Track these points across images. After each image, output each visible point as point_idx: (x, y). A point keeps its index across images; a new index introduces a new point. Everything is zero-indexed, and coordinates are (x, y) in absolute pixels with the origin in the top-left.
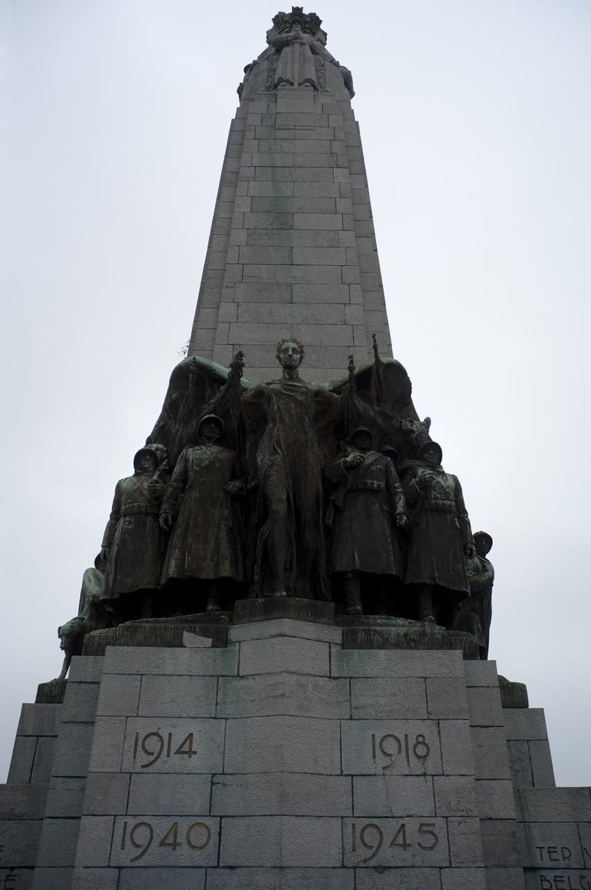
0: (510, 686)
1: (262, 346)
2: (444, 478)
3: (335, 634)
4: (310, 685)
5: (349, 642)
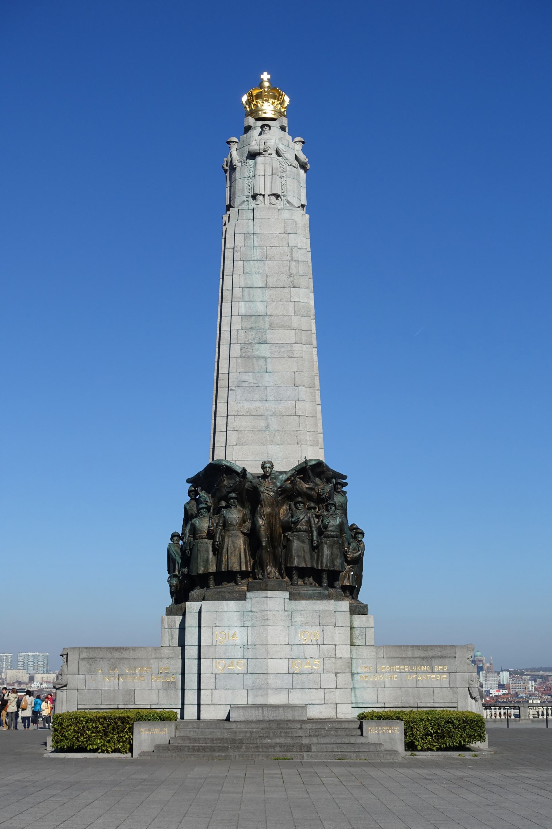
3: (287, 594)
5: (293, 597)
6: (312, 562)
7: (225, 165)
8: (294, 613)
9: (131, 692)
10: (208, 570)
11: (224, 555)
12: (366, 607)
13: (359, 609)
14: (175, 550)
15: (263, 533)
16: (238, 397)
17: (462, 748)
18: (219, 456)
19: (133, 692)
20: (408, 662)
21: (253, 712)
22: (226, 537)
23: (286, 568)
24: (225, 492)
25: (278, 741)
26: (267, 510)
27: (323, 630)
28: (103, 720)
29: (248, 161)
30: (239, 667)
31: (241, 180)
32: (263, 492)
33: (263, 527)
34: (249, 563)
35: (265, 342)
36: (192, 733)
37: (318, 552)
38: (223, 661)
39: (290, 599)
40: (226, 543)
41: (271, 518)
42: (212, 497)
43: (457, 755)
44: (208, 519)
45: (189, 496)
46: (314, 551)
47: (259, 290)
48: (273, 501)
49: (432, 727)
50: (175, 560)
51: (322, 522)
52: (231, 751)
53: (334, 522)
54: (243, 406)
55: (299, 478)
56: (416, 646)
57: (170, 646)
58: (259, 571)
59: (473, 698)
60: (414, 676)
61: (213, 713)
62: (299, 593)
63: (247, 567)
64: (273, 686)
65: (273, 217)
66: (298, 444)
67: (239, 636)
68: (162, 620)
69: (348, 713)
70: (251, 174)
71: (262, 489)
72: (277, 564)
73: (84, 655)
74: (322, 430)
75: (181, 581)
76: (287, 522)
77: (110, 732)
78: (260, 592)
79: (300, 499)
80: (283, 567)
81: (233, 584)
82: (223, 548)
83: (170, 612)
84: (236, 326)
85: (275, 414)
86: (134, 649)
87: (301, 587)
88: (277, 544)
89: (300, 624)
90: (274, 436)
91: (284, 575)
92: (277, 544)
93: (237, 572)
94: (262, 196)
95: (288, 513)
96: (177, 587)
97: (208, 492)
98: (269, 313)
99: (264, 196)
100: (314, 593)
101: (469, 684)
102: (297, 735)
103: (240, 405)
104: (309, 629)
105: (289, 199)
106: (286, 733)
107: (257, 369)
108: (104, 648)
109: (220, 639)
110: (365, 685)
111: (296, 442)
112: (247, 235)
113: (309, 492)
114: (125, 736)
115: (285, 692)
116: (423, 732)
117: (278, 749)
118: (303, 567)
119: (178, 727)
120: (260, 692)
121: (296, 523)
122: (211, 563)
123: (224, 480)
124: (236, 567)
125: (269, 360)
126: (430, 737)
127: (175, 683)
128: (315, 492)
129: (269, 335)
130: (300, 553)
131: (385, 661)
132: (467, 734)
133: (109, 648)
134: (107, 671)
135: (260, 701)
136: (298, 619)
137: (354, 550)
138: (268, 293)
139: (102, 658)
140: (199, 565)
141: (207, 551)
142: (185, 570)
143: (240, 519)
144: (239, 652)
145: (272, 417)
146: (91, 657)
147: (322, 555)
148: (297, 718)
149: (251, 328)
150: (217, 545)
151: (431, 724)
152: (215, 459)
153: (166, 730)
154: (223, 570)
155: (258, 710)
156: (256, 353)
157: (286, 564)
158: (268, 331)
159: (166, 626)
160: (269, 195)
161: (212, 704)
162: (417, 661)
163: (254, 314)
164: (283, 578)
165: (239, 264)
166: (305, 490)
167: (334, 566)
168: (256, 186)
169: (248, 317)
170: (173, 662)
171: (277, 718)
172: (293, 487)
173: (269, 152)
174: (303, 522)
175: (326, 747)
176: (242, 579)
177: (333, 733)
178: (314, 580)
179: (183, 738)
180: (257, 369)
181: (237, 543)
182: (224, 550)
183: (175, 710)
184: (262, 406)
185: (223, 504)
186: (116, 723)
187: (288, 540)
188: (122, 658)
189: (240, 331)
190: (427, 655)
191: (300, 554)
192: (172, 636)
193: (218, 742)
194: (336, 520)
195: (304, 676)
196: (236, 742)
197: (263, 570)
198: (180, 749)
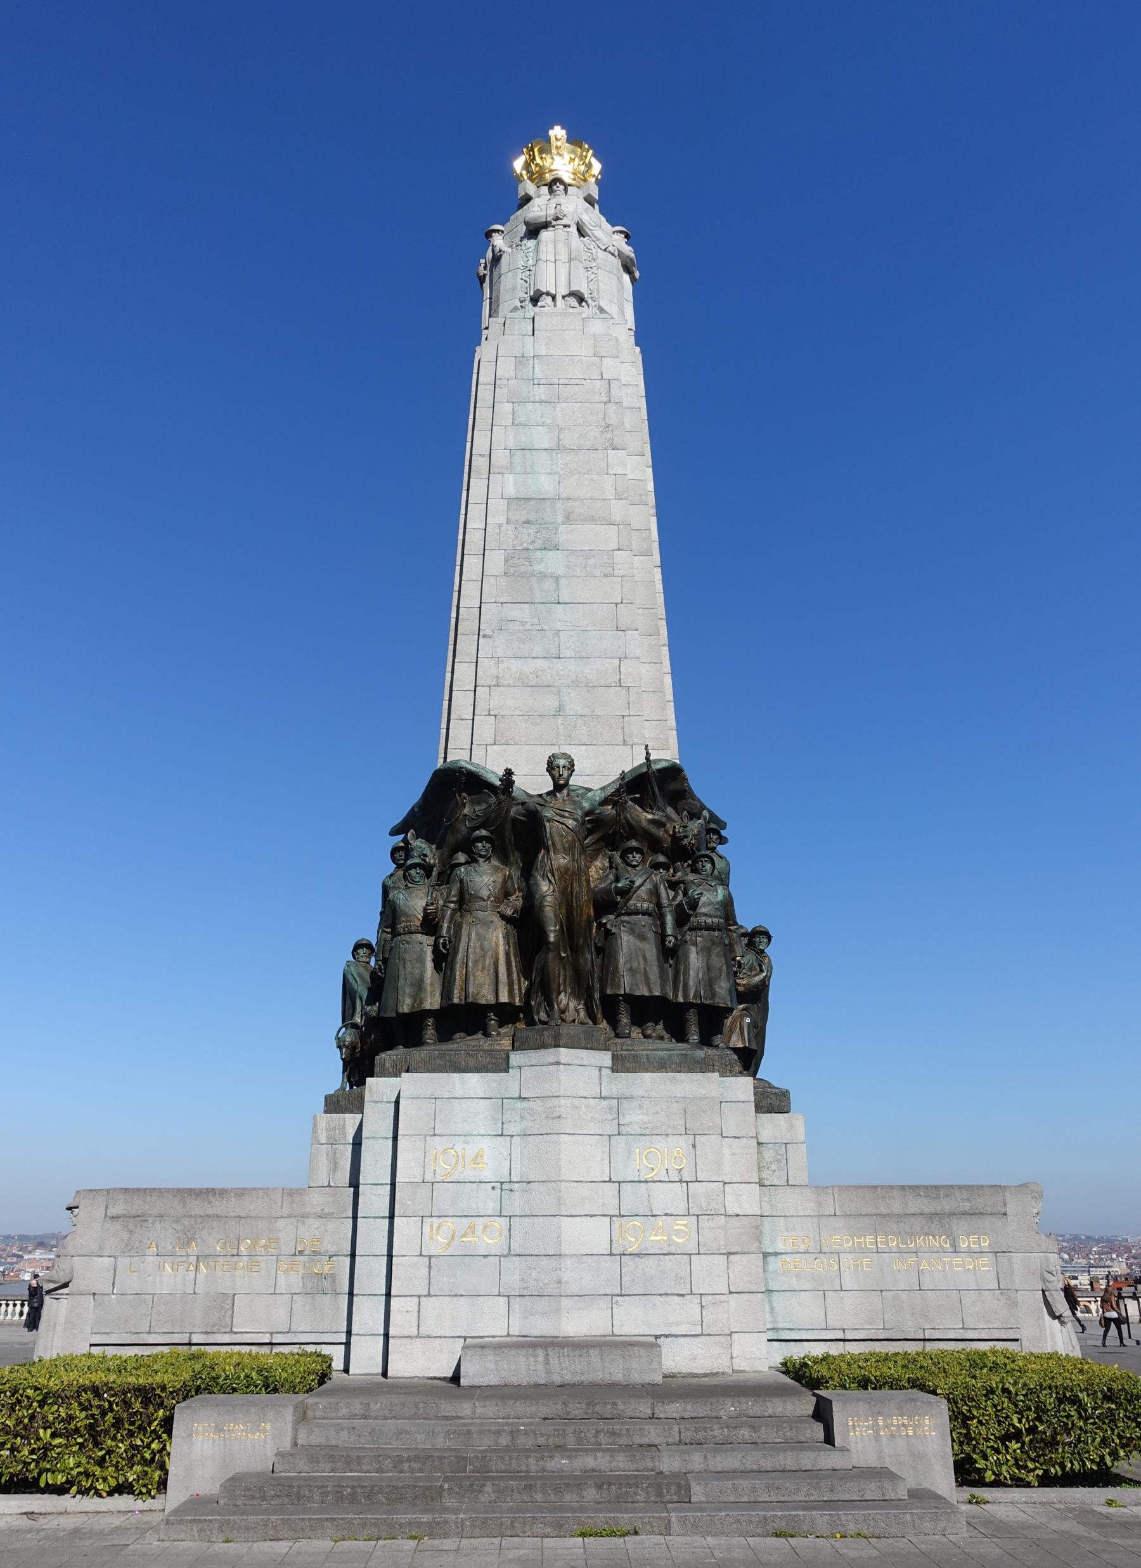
3: (606, 1058)
6: (663, 986)
7: (481, 268)
8: (625, 1104)
9: (226, 1302)
10: (421, 1003)
11: (458, 966)
12: (784, 1095)
13: (771, 1101)
14: (360, 975)
15: (549, 913)
16: (498, 650)
17: (1103, 1477)
18: (458, 755)
19: (229, 1301)
20: (895, 1226)
21: (522, 1360)
22: (464, 926)
23: (604, 998)
25: (589, 1462)
26: (561, 860)
27: (694, 1146)
28: (90, 1395)
29: (525, 241)
30: (489, 1238)
31: (510, 274)
32: (549, 821)
33: (549, 898)
34: (516, 987)
35: (556, 548)
36: (344, 1434)
37: (677, 963)
38: (449, 1223)
39: (614, 1069)
40: (464, 939)
41: (568, 879)
42: (437, 848)
43: (1103, 1500)
45: (394, 860)
46: (667, 961)
47: (544, 454)
48: (574, 841)
49: (1020, 1413)
50: (356, 992)
51: (685, 894)
52: (449, 1502)
53: (709, 898)
54: (508, 668)
56: (910, 1187)
57: (329, 1186)
58: (539, 1005)
59: (1054, 1316)
60: (912, 1260)
61: (416, 1362)
62: (635, 1057)
64: (573, 1288)
65: (571, 327)
66: (625, 743)
67: (488, 1157)
68: (315, 1125)
69: (758, 1358)
70: (531, 262)
71: (548, 813)
72: (582, 991)
73: (118, 1209)
74: (674, 723)
75: (363, 1037)
76: (607, 891)
77: (107, 1432)
80: (597, 996)
81: (480, 1035)
82: (456, 952)
83: (333, 1105)
84: (498, 517)
85: (576, 683)
86: (240, 1193)
87: (637, 1042)
89: (638, 1131)
90: (575, 726)
91: (600, 1016)
93: (488, 1007)
94: (550, 298)
97: (429, 840)
98: (563, 495)
99: (554, 298)
100: (670, 1056)
101: (1044, 1280)
102: (644, 1441)
103: (502, 666)
104: (661, 1143)
105: (602, 304)
106: (613, 1433)
107: (538, 596)
108: (168, 1190)
109: (442, 1168)
110: (795, 1284)
111: (620, 739)
112: (521, 360)
113: (654, 830)
114: (148, 1446)
115: (604, 1303)
116: (995, 1430)
117: (591, 1494)
118: (643, 996)
119: (310, 1413)
120: (540, 1304)
121: (626, 893)
122: (429, 989)
123: (465, 807)
125: (563, 581)
126: (1014, 1445)
127: (333, 1277)
128: (666, 832)
129: (566, 535)
131: (839, 1223)
132: (1120, 1437)
133: (179, 1190)
134: (170, 1247)
135: (540, 1327)
136: (634, 1118)
137: (751, 969)
138: (561, 459)
139: (161, 1216)
140: (400, 992)
141: (421, 961)
142: (373, 1010)
144: (488, 1201)
145: (569, 690)
146: (134, 1212)
147: (687, 970)
148: (637, 1378)
149: (528, 522)
150: (444, 945)
151: (1016, 1406)
153: (268, 1427)
154: (456, 1001)
155: (536, 1356)
156: (538, 568)
158: (562, 528)
159: (323, 1140)
160: (564, 297)
161: (418, 1336)
162: (918, 1223)
163: (534, 496)
164: (595, 1023)
165: (504, 408)
166: (644, 824)
167: (714, 995)
168: (539, 278)
169: (522, 502)
170: (331, 1225)
171: (584, 1378)
172: (618, 814)
173: (564, 222)
174: (642, 893)
175: (736, 1488)
176: (501, 1025)
177: (745, 1433)
179: (313, 1453)
180: (538, 596)
181: (488, 941)
182: (460, 956)
183: (326, 1350)
184: (550, 668)
185: (461, 857)
186: (127, 1404)
187: (608, 934)
188: (209, 1216)
189: (505, 527)
190: (939, 1209)
191: (635, 965)
192: (336, 1163)
193: (416, 1465)
195: (651, 1261)
196: (470, 1468)
197: (549, 1001)
198: (299, 1496)
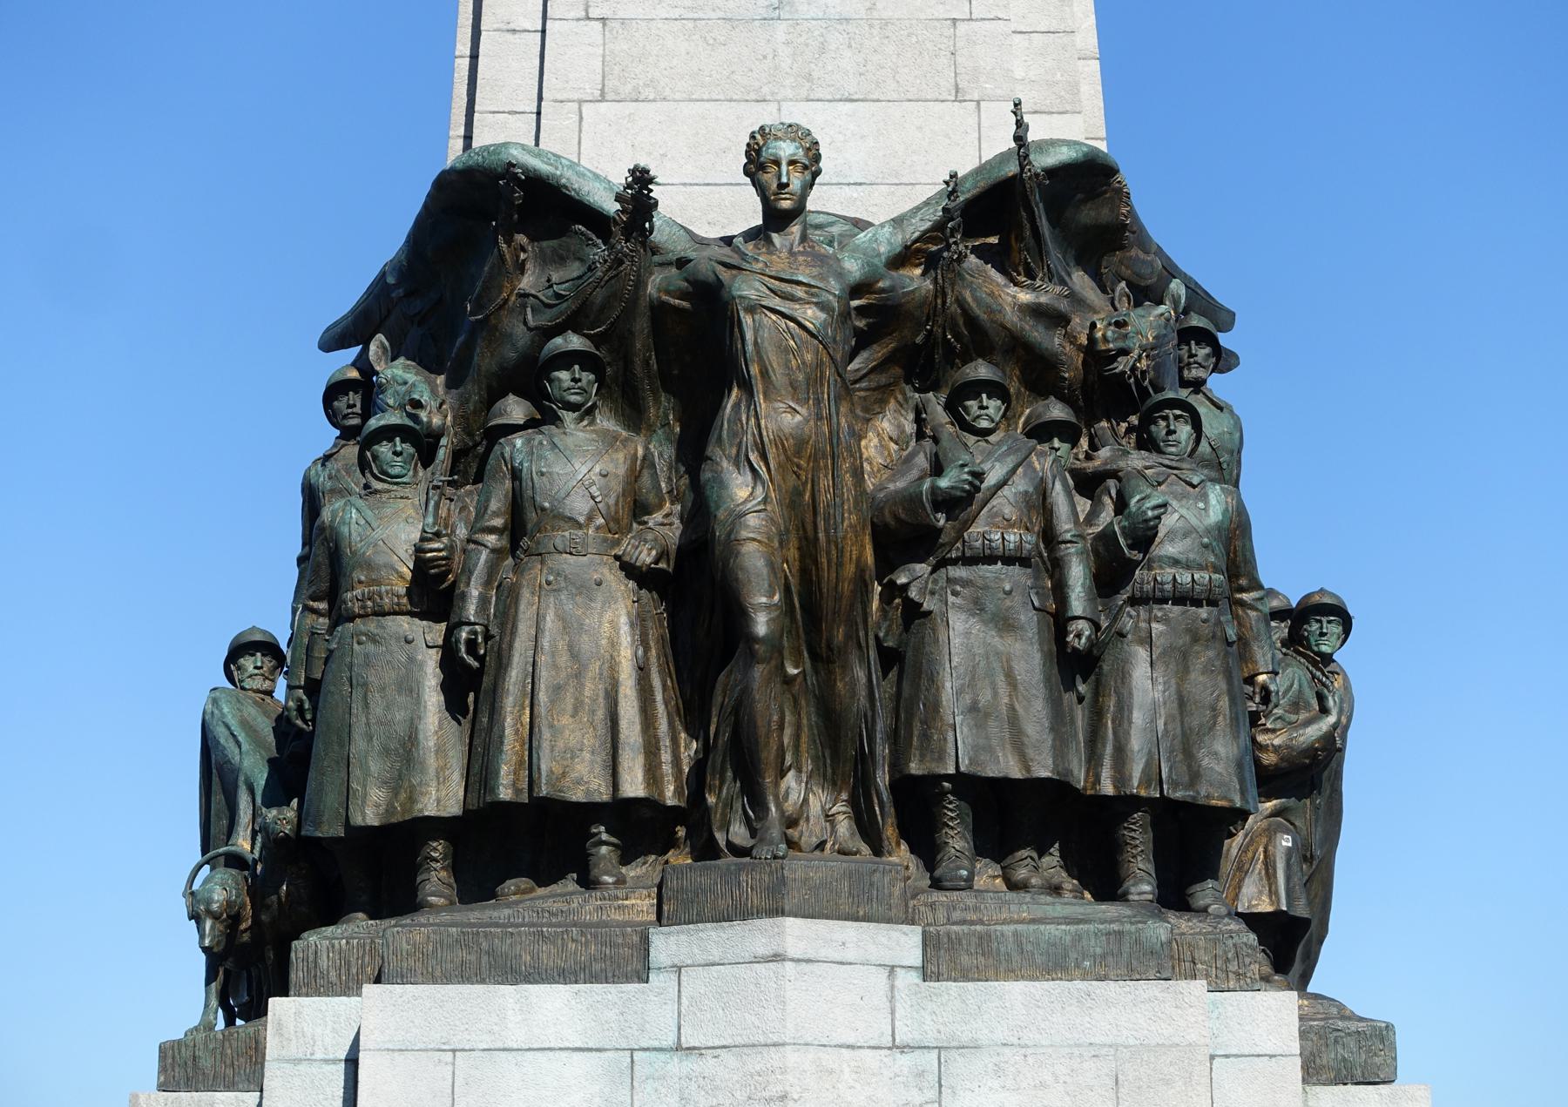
0: (304, 990)
1: (690, 25)
2: (1201, 505)
3: (905, 943)
4: (847, 1070)
6: (1060, 750)
8: (958, 1064)
10: (412, 800)
12: (1382, 1036)
14: (244, 724)
18: (503, 131)
22: (526, 594)
23: (904, 786)
24: (521, 335)
26: (784, 417)
33: (753, 520)
34: (666, 756)
37: (1097, 693)
40: (525, 629)
41: (804, 470)
42: (450, 385)
44: (417, 498)
45: (332, 416)
46: (1070, 686)
48: (820, 365)
50: (236, 771)
53: (1186, 519)
55: (980, 252)
58: (729, 805)
63: (652, 773)
66: (958, 95)
72: (844, 765)
75: (258, 890)
76: (910, 500)
78: (737, 929)
79: (982, 370)
80: (882, 779)
81: (570, 884)
82: (502, 665)
88: (840, 634)
90: (823, 49)
91: (890, 832)
92: (840, 634)
93: (589, 812)
95: (908, 460)
96: (235, 919)
97: (429, 363)
100: (1078, 938)
111: (947, 84)
121: (960, 504)
122: (432, 762)
123: (521, 267)
124: (584, 781)
128: (1071, 338)
130: (985, 689)
137: (1296, 706)
140: (356, 772)
141: (409, 687)
142: (283, 818)
143: (617, 487)
147: (1123, 709)
150: (472, 645)
152: (476, 144)
154: (505, 794)
157: (897, 764)
164: (878, 851)
166: (1011, 317)
167: (1195, 776)
172: (940, 292)
174: (1006, 503)
176: (626, 859)
178: (1069, 864)
181: (588, 646)
185: (515, 409)
187: (914, 613)
191: (985, 697)
194: (1204, 497)
